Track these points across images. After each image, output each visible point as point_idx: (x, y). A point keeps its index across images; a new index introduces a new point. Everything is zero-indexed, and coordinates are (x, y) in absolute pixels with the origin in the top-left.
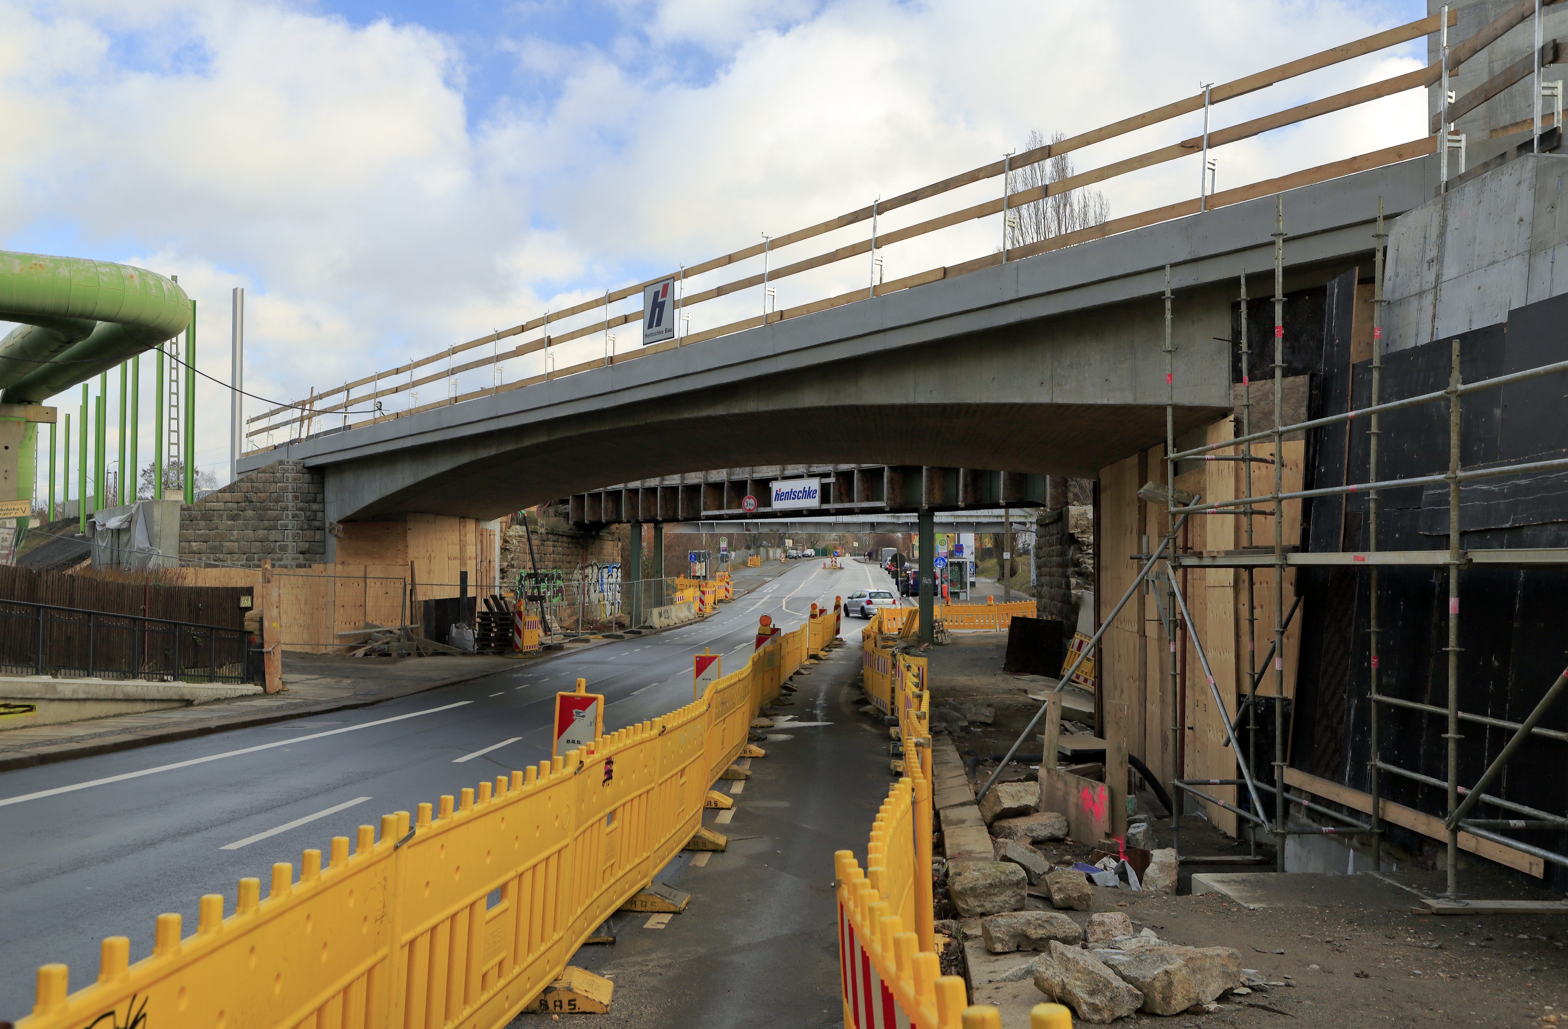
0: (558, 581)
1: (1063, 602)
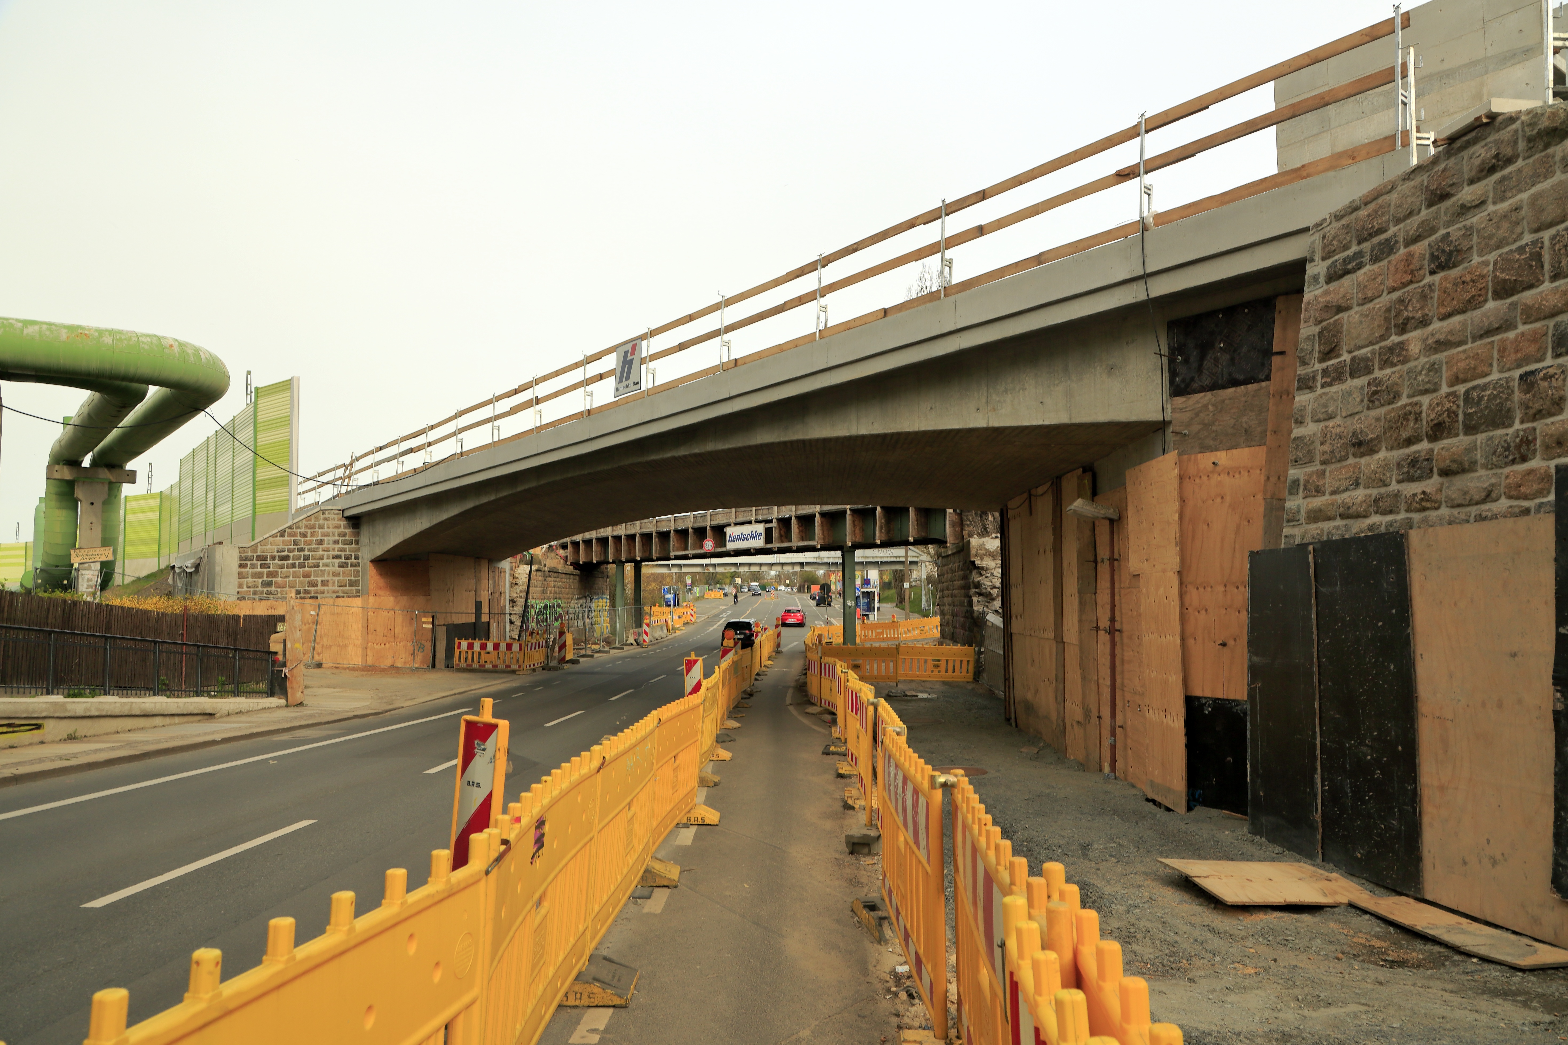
0: (558, 609)
1: (965, 617)
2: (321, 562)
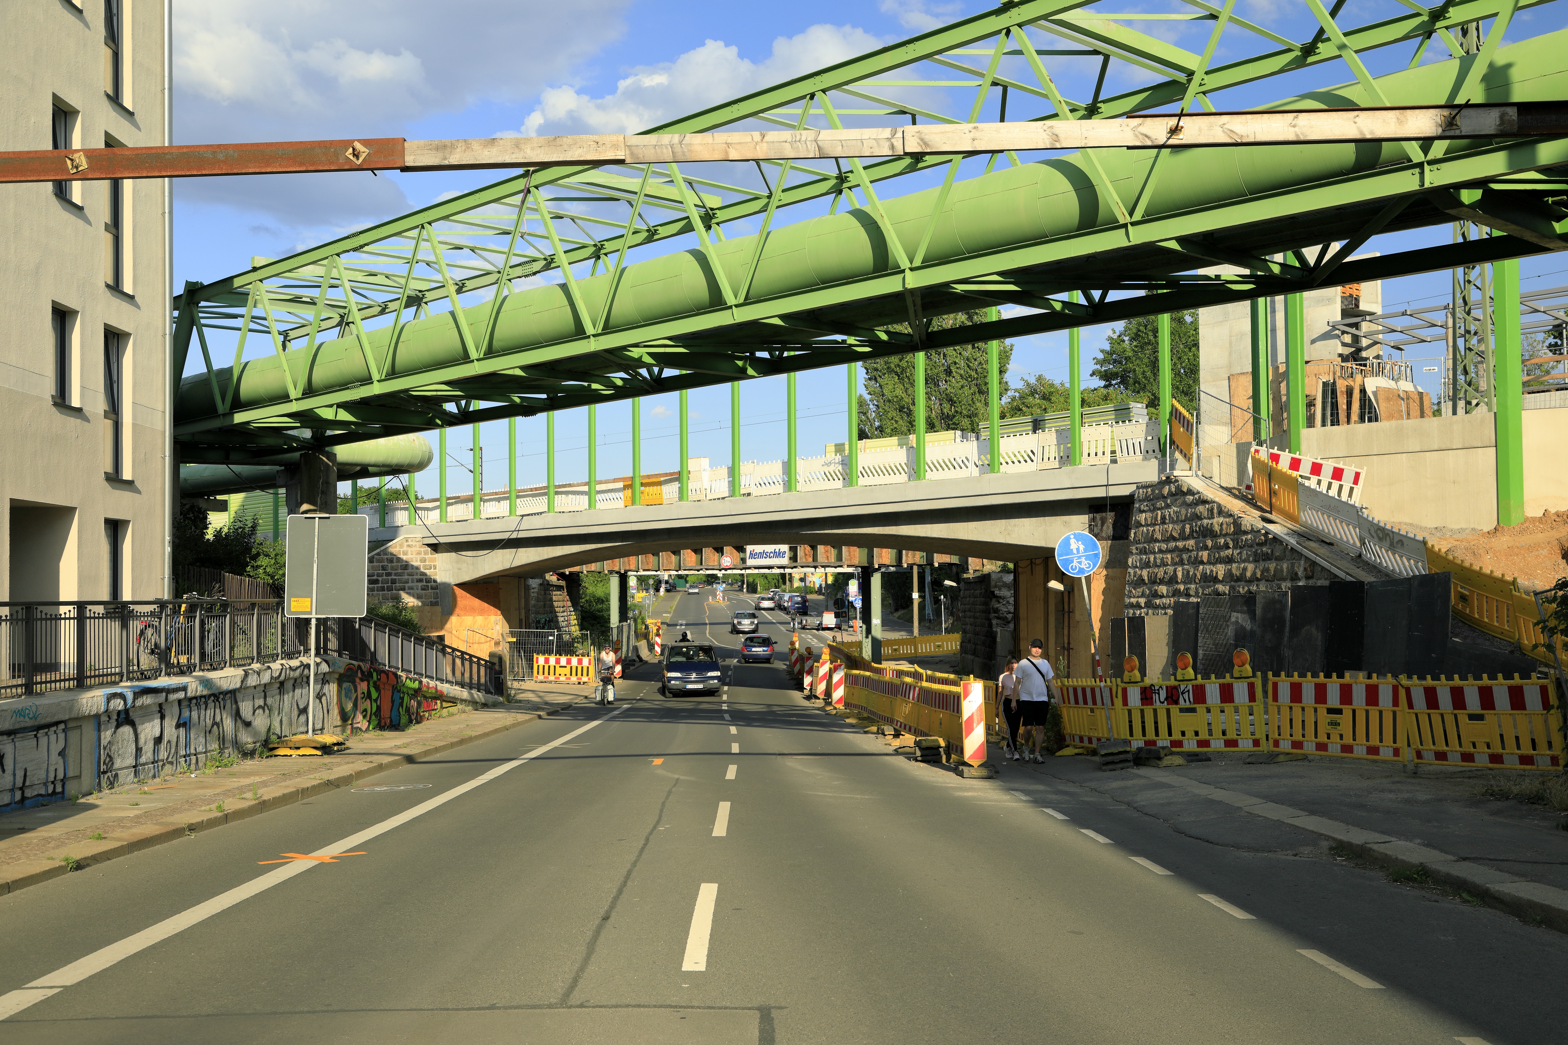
2: (407, 585)
